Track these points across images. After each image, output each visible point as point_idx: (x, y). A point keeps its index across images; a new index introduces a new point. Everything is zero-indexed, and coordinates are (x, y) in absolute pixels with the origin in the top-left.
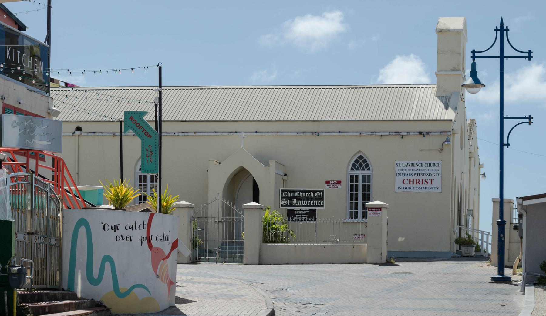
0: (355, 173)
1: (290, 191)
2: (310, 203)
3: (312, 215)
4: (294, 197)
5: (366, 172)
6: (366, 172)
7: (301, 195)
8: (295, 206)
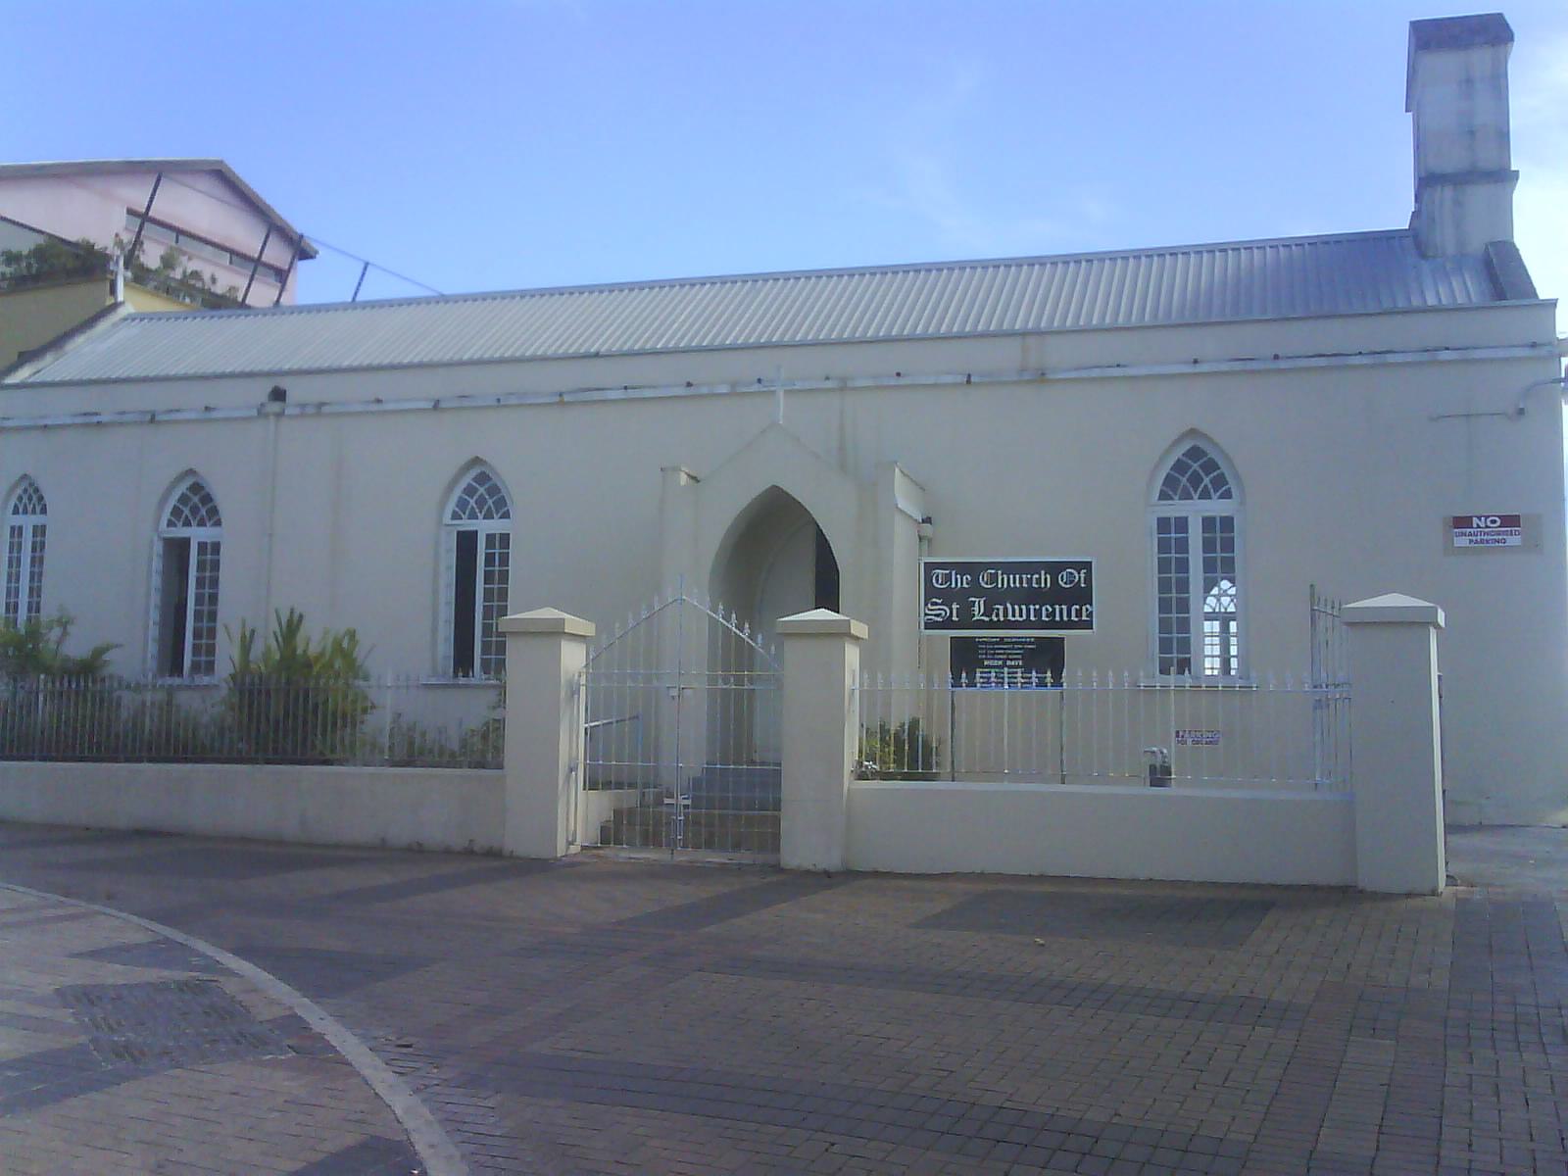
0: (1175, 509)
1: (963, 568)
2: (1038, 613)
3: (1047, 658)
4: (975, 590)
5: (1216, 507)
6: (1216, 507)
7: (1004, 581)
8: (980, 625)
